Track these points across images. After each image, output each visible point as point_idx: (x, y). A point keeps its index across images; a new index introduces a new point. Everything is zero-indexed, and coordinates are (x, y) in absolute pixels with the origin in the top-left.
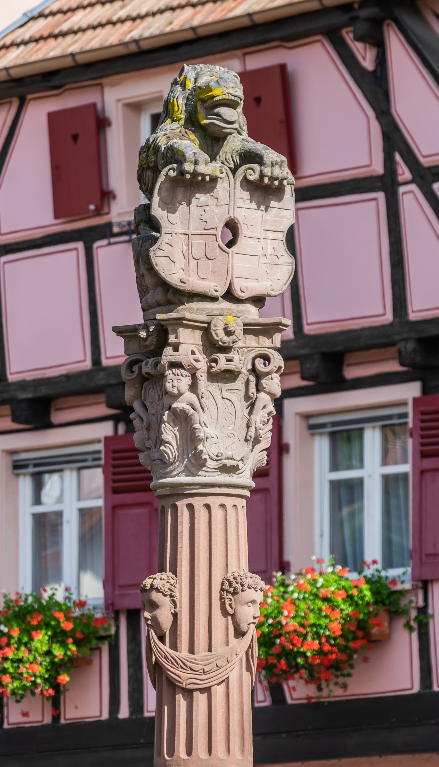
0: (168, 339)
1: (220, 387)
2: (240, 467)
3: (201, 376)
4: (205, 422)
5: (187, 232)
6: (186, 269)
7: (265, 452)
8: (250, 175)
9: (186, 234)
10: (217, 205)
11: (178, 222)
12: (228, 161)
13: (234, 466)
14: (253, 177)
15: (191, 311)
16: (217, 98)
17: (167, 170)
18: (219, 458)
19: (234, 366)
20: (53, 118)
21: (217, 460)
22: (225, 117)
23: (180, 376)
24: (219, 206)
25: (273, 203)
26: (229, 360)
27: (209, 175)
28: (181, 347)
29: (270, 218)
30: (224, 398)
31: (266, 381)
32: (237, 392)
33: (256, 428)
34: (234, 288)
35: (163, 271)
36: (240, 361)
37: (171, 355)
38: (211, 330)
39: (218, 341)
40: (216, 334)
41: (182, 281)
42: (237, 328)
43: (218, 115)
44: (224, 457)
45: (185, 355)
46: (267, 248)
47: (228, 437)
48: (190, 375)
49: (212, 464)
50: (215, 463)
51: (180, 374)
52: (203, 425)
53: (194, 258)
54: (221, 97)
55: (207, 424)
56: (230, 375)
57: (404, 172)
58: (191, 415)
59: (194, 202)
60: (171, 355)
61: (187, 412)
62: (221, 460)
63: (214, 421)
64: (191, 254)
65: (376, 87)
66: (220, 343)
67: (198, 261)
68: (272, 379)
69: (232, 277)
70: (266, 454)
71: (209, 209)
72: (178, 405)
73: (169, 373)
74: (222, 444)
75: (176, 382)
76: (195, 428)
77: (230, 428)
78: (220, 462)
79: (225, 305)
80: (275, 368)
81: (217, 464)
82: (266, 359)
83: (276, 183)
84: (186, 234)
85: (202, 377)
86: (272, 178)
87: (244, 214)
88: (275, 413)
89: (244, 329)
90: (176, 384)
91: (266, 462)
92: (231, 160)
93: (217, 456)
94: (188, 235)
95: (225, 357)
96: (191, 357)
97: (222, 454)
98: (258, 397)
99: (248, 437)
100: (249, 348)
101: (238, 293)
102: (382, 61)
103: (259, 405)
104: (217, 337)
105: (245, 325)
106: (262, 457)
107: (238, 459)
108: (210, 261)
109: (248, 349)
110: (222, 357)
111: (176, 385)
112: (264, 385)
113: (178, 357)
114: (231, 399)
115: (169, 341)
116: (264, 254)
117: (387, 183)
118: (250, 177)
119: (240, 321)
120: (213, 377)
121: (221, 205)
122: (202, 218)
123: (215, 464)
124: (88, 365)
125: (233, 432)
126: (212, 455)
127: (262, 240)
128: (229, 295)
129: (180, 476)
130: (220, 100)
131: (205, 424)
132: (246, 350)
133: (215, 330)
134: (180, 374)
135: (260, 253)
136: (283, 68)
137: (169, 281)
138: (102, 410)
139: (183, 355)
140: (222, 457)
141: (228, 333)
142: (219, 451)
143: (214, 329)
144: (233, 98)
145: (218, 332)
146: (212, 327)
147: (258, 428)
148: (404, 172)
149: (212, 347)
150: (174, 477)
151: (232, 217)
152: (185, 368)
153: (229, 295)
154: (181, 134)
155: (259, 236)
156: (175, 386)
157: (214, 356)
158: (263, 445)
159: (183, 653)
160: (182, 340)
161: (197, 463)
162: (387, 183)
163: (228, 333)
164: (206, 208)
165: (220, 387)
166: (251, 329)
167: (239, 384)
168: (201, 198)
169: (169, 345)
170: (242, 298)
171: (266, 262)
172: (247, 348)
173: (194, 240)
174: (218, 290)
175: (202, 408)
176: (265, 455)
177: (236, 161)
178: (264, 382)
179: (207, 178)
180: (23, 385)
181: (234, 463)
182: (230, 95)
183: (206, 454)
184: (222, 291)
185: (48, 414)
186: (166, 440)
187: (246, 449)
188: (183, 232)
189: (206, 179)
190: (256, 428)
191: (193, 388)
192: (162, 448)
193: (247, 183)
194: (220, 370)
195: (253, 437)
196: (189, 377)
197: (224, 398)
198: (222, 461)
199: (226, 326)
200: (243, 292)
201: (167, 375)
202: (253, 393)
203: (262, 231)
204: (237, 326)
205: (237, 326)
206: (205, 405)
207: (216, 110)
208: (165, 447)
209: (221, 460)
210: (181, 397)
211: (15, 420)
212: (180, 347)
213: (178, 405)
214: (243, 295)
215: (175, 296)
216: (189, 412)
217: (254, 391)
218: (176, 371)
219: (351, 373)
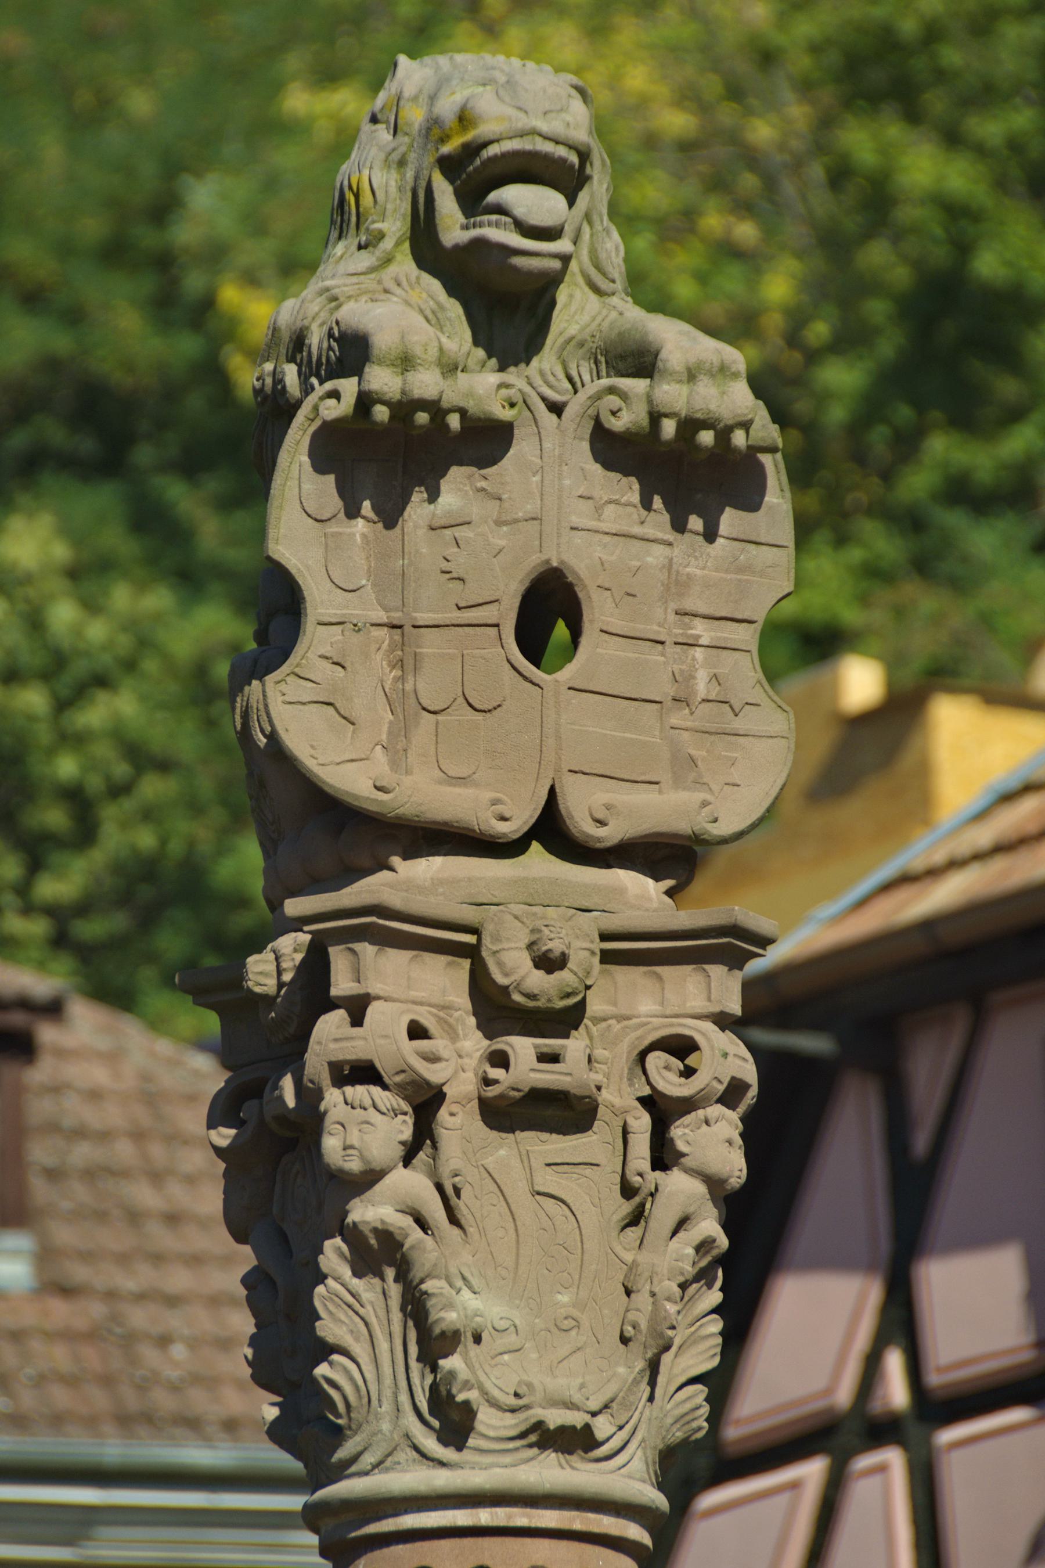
0: (329, 986)
1: (524, 1153)
2: (600, 1435)
3: (452, 1114)
4: (467, 1275)
5: (397, 617)
6: (396, 749)
7: (699, 1387)
8: (614, 413)
9: (395, 627)
10: (499, 523)
11: (364, 582)
12: (551, 378)
13: (574, 1427)
14: (627, 419)
16: (493, 150)
17: (316, 399)
18: (521, 1402)
19: (568, 1079)
21: (513, 1411)
22: (519, 212)
23: (371, 1110)
24: (505, 523)
25: (730, 520)
26: (551, 1058)
27: (463, 412)
28: (374, 1012)
29: (698, 572)
30: (539, 1193)
31: (687, 1131)
32: (588, 1171)
33: (653, 1294)
34: (567, 808)
35: (313, 752)
36: (585, 1061)
37: (336, 1040)
38: (484, 954)
39: (505, 989)
40: (500, 964)
41: (378, 784)
42: (578, 944)
43: (500, 210)
44: (539, 1396)
45: (386, 1037)
46: (694, 678)
47: (555, 1330)
48: (410, 1110)
49: (499, 1423)
50: (510, 1419)
51: (368, 1102)
52: (459, 1283)
53: (424, 709)
54: (508, 146)
55: (474, 1281)
56: (563, 1111)
58: (412, 1247)
59: (418, 510)
60: (336, 1040)
61: (398, 1238)
62: (527, 1407)
63: (504, 1273)
64: (412, 696)
66: (517, 997)
67: (440, 717)
68: (707, 1123)
69: (558, 770)
70: (703, 1396)
71: (471, 535)
72: (368, 1212)
73: (333, 1097)
74: (534, 1356)
75: (356, 1132)
76: (426, 1293)
77: (564, 1298)
78: (521, 1416)
79: (538, 861)
80: (715, 1084)
81: (513, 1422)
82: (681, 1047)
83: (706, 438)
84: (395, 627)
85: (458, 1124)
86: (690, 426)
87: (599, 553)
88: (723, 1242)
89: (603, 952)
90: (354, 1138)
91: (705, 1424)
92: (561, 375)
93: (516, 1395)
94: (400, 627)
95: (536, 1047)
96: (410, 1049)
97: (530, 1385)
98: (660, 1188)
99: (629, 1331)
100: (629, 1018)
101: (580, 821)
103: (661, 1217)
104: (506, 975)
105: (604, 937)
106: (688, 1406)
107: (594, 1405)
108: (479, 717)
109: (626, 1023)
110: (523, 1048)
111: (356, 1144)
112: (681, 1146)
113: (361, 1043)
114: (563, 1197)
115: (334, 992)
116: (682, 695)
118: (613, 419)
119: (591, 924)
120: (503, 1114)
121: (516, 521)
122: (445, 566)
123: (512, 1424)
125: (575, 1313)
126: (496, 1393)
127: (670, 649)
128: (551, 830)
129: (387, 1470)
130: (504, 156)
131: (464, 1278)
132: (616, 1026)
133: (495, 953)
134: (368, 1102)
135: (665, 689)
137: (331, 786)
139: (381, 1037)
140: (533, 1399)
141: (549, 963)
142: (525, 1378)
143: (495, 948)
144: (548, 147)
145: (505, 957)
146: (486, 941)
147: (659, 1295)
149: (497, 1011)
150: (367, 1473)
151: (555, 564)
152: (386, 1079)
153: (551, 830)
154: (380, 288)
155: (653, 630)
156: (352, 1147)
157: (502, 1043)
158: (691, 1362)
160: (374, 987)
161: (453, 1422)
163: (549, 963)
164: (460, 532)
165: (524, 1153)
166: (628, 950)
167: (594, 1144)
168: (457, 488)
169: (331, 1005)
170: (598, 845)
171: (689, 724)
172: (621, 1018)
173: (431, 644)
174: (507, 815)
175: (454, 1219)
176: (700, 1399)
177: (577, 379)
178: (682, 1133)
179: (454, 421)
181: (577, 1419)
182: (538, 139)
183: (467, 1385)
186: (330, 1339)
187: (621, 1370)
188: (382, 616)
189: (447, 426)
190: (653, 1294)
191: (423, 1136)
192: (322, 1370)
193: (611, 448)
194: (518, 1090)
195: (644, 1325)
196: (405, 1114)
197: (539, 1193)
198: (531, 1412)
199: (534, 937)
200: (602, 823)
201: (326, 1112)
202: (641, 1175)
203: (672, 617)
206: (470, 1216)
207: (493, 197)
208: (331, 1364)
209: (527, 1407)
210: (378, 1188)
212: (370, 1011)
213: (368, 1212)
214: (601, 832)
215: (357, 835)
216: (406, 1236)
217: (645, 1165)
218: (359, 1092)
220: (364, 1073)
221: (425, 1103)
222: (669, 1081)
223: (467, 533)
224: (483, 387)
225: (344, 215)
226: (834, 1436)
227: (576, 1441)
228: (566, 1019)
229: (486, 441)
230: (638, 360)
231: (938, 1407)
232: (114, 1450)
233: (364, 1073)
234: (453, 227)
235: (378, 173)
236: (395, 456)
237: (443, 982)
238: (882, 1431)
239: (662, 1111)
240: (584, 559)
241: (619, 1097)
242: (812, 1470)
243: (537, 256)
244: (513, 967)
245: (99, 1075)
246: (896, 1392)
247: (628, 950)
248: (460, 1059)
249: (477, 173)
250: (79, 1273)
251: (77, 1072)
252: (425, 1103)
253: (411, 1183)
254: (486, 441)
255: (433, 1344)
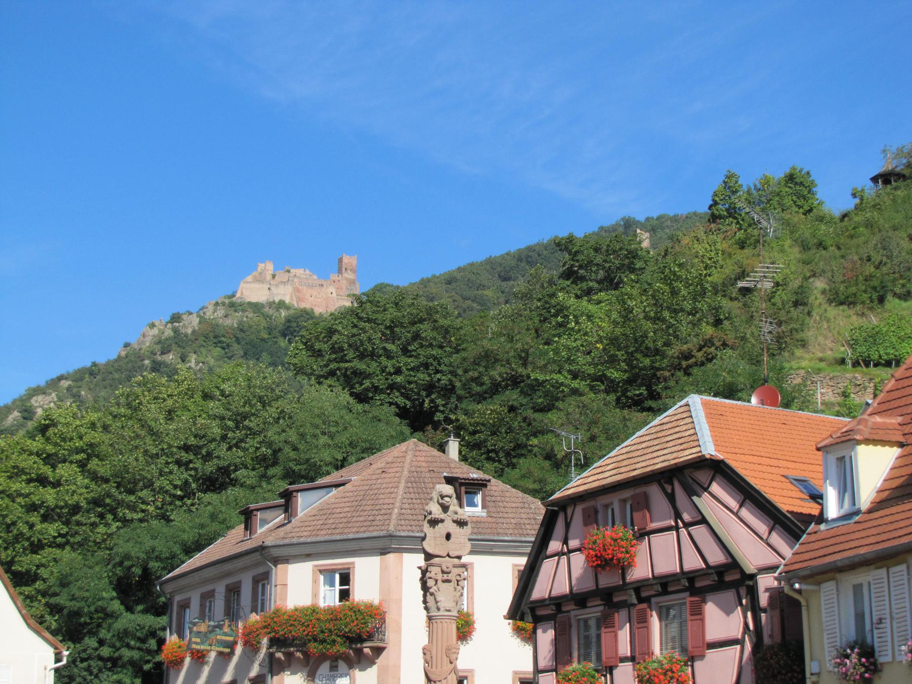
15: (436, 560)
20: (583, 510)
36: (450, 577)
56: (448, 581)
57: (681, 524)
65: (671, 498)
85: (439, 582)
102: (673, 490)
117: (677, 528)
120: (444, 581)
124: (594, 588)
128: (448, 555)
136: (645, 493)
138: (600, 602)
139: (432, 575)
148: (681, 524)
149: (443, 572)
153: (448, 555)
159: (434, 669)
161: (439, 609)
162: (677, 528)
166: (455, 566)
168: (440, 525)
180: (577, 594)
184: (445, 554)
185: (586, 603)
193: (454, 521)
204: (450, 565)
205: (450, 565)
211: (576, 605)
213: (431, 590)
219: (670, 589)
220: (430, 578)
221: (436, 581)
222: (458, 578)
223: (441, 529)
224: (443, 516)
225: (431, 499)
226: (559, 554)
227: (449, 611)
228: (449, 573)
229: (442, 521)
230: (456, 513)
231: (570, 551)
232: (496, 538)
233: (430, 578)
234: (441, 501)
235: (435, 496)
236: (434, 523)
237: (439, 569)
238: (563, 554)
239: (458, 581)
240: (451, 531)
241: (454, 579)
242: (557, 558)
243: (447, 504)
244: (445, 569)
245: (496, 488)
246: (566, 550)
247: (455, 566)
248: (440, 577)
249: (442, 497)
250: (493, 515)
251: (494, 488)
252: (436, 581)
253: (435, 588)
254: (442, 521)
255: (437, 602)
